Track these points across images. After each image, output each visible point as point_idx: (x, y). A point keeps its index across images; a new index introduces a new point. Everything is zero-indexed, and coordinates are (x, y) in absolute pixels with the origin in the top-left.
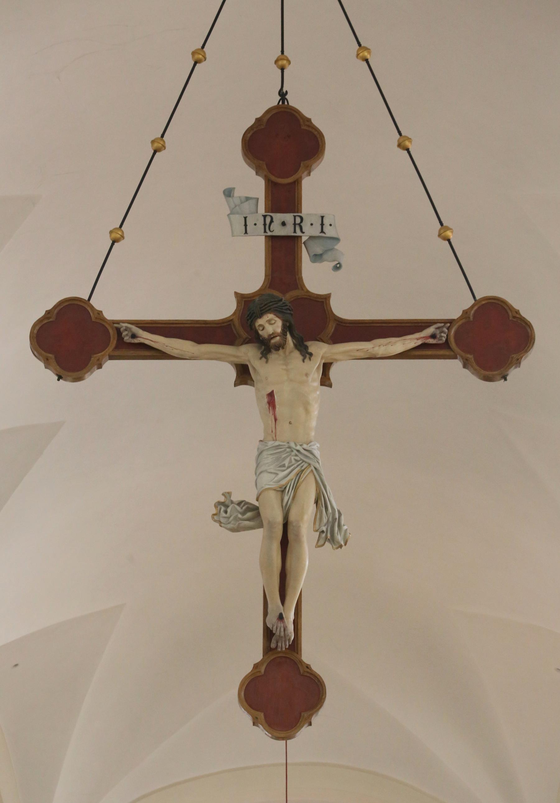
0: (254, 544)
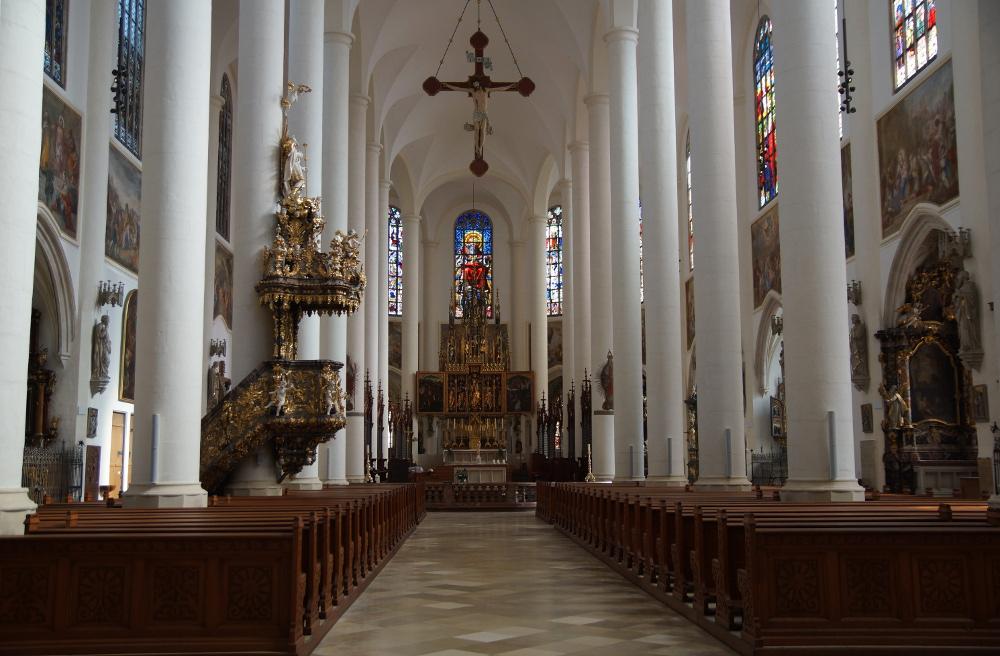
0: (473, 134)
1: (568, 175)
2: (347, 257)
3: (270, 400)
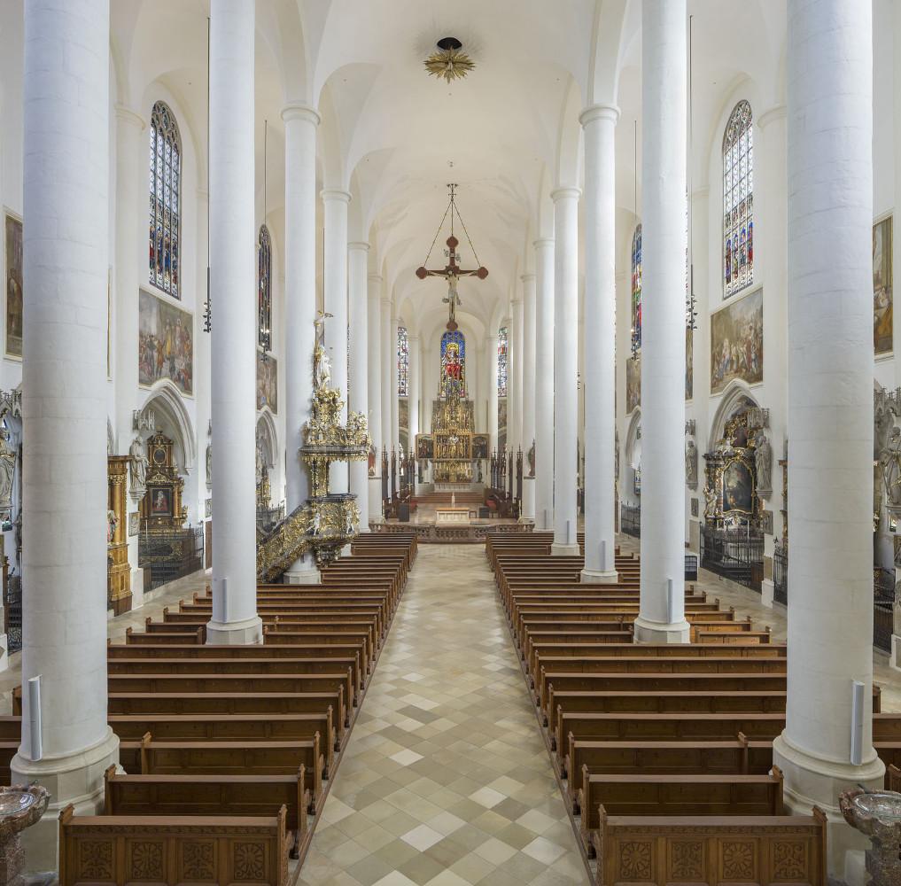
1: (511, 316)
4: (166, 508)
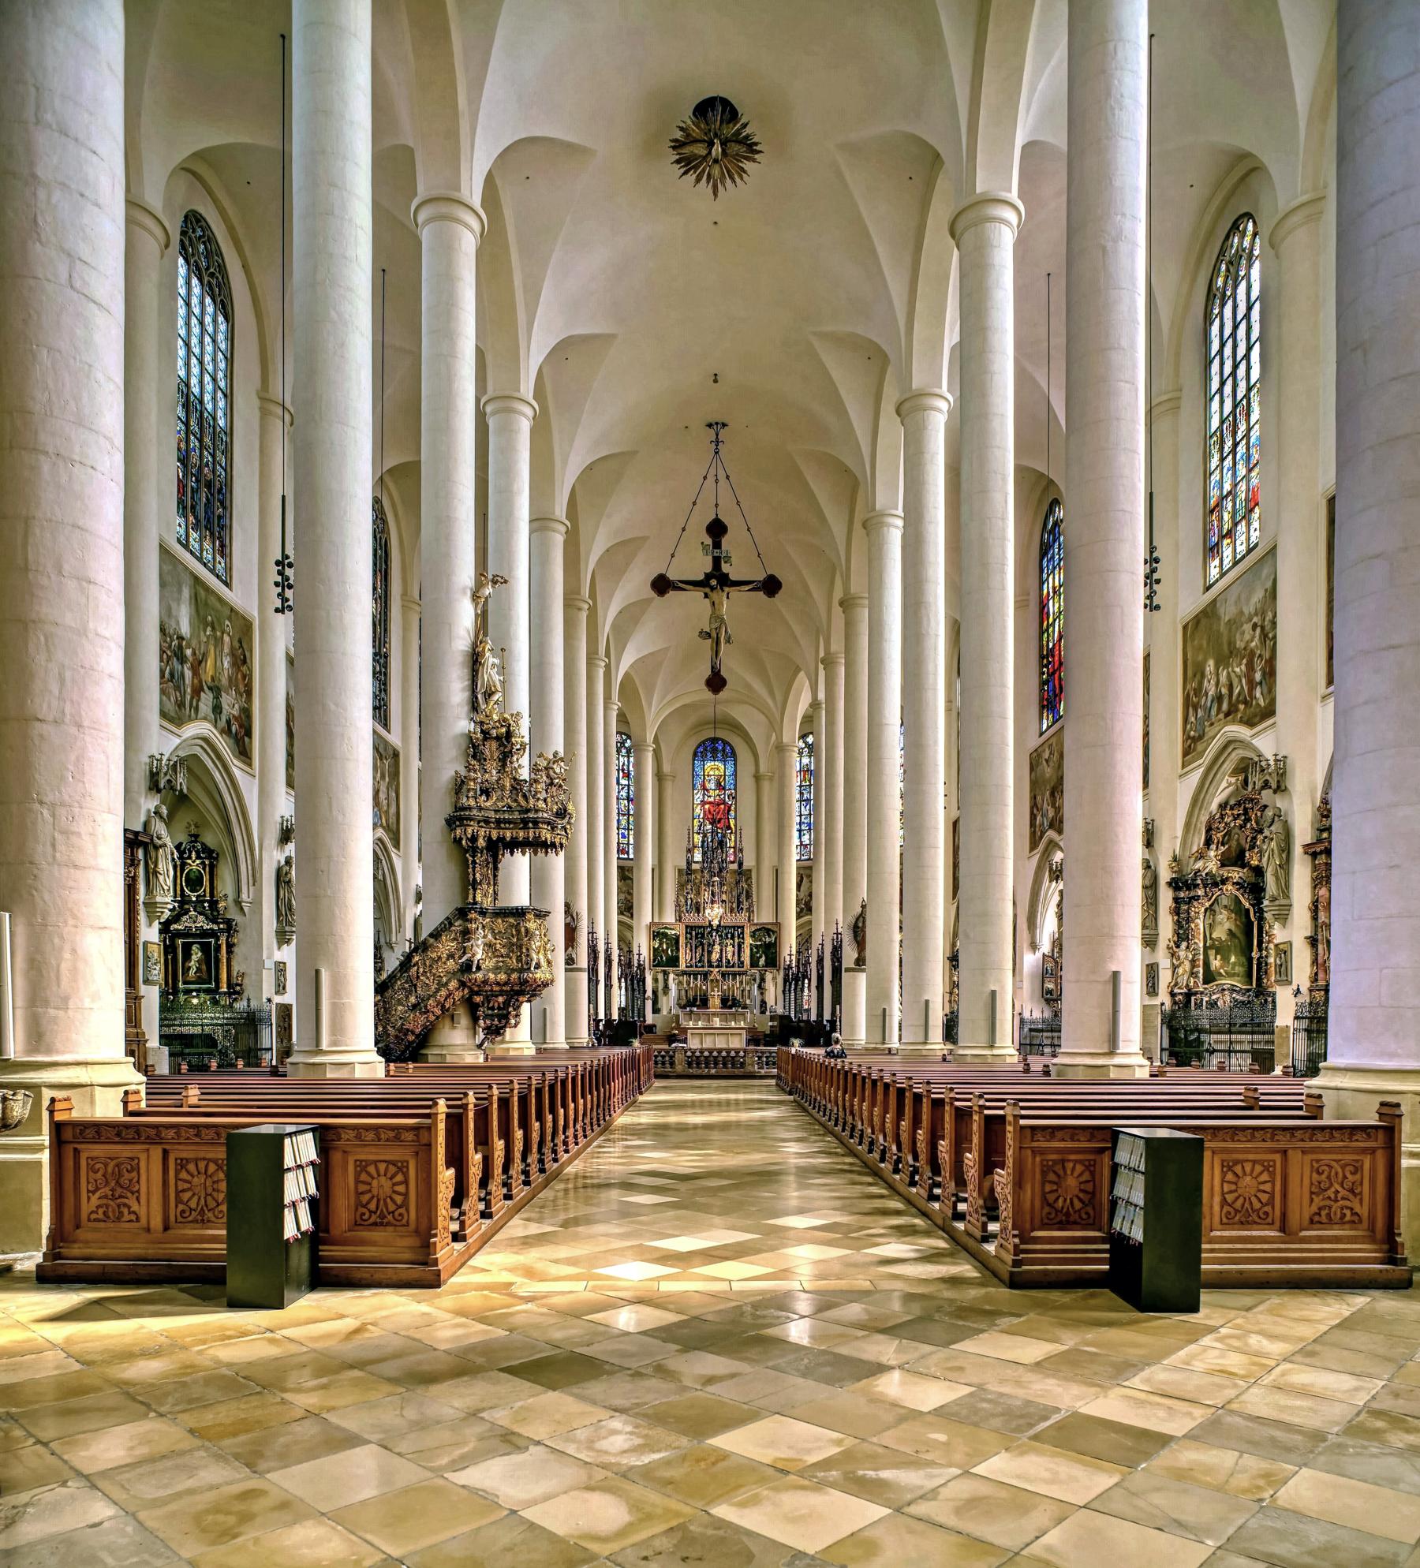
1: (821, 696)
2: (551, 784)
3: (464, 953)
4: (205, 976)
